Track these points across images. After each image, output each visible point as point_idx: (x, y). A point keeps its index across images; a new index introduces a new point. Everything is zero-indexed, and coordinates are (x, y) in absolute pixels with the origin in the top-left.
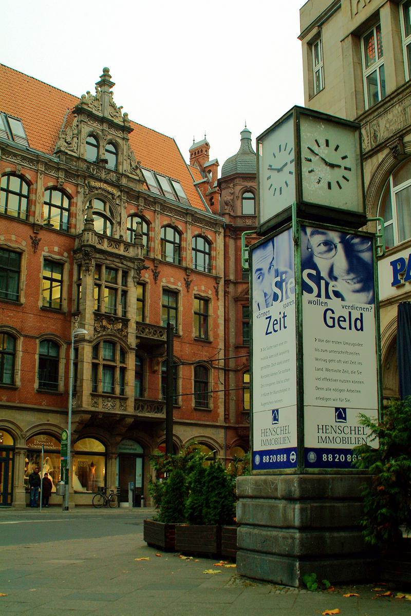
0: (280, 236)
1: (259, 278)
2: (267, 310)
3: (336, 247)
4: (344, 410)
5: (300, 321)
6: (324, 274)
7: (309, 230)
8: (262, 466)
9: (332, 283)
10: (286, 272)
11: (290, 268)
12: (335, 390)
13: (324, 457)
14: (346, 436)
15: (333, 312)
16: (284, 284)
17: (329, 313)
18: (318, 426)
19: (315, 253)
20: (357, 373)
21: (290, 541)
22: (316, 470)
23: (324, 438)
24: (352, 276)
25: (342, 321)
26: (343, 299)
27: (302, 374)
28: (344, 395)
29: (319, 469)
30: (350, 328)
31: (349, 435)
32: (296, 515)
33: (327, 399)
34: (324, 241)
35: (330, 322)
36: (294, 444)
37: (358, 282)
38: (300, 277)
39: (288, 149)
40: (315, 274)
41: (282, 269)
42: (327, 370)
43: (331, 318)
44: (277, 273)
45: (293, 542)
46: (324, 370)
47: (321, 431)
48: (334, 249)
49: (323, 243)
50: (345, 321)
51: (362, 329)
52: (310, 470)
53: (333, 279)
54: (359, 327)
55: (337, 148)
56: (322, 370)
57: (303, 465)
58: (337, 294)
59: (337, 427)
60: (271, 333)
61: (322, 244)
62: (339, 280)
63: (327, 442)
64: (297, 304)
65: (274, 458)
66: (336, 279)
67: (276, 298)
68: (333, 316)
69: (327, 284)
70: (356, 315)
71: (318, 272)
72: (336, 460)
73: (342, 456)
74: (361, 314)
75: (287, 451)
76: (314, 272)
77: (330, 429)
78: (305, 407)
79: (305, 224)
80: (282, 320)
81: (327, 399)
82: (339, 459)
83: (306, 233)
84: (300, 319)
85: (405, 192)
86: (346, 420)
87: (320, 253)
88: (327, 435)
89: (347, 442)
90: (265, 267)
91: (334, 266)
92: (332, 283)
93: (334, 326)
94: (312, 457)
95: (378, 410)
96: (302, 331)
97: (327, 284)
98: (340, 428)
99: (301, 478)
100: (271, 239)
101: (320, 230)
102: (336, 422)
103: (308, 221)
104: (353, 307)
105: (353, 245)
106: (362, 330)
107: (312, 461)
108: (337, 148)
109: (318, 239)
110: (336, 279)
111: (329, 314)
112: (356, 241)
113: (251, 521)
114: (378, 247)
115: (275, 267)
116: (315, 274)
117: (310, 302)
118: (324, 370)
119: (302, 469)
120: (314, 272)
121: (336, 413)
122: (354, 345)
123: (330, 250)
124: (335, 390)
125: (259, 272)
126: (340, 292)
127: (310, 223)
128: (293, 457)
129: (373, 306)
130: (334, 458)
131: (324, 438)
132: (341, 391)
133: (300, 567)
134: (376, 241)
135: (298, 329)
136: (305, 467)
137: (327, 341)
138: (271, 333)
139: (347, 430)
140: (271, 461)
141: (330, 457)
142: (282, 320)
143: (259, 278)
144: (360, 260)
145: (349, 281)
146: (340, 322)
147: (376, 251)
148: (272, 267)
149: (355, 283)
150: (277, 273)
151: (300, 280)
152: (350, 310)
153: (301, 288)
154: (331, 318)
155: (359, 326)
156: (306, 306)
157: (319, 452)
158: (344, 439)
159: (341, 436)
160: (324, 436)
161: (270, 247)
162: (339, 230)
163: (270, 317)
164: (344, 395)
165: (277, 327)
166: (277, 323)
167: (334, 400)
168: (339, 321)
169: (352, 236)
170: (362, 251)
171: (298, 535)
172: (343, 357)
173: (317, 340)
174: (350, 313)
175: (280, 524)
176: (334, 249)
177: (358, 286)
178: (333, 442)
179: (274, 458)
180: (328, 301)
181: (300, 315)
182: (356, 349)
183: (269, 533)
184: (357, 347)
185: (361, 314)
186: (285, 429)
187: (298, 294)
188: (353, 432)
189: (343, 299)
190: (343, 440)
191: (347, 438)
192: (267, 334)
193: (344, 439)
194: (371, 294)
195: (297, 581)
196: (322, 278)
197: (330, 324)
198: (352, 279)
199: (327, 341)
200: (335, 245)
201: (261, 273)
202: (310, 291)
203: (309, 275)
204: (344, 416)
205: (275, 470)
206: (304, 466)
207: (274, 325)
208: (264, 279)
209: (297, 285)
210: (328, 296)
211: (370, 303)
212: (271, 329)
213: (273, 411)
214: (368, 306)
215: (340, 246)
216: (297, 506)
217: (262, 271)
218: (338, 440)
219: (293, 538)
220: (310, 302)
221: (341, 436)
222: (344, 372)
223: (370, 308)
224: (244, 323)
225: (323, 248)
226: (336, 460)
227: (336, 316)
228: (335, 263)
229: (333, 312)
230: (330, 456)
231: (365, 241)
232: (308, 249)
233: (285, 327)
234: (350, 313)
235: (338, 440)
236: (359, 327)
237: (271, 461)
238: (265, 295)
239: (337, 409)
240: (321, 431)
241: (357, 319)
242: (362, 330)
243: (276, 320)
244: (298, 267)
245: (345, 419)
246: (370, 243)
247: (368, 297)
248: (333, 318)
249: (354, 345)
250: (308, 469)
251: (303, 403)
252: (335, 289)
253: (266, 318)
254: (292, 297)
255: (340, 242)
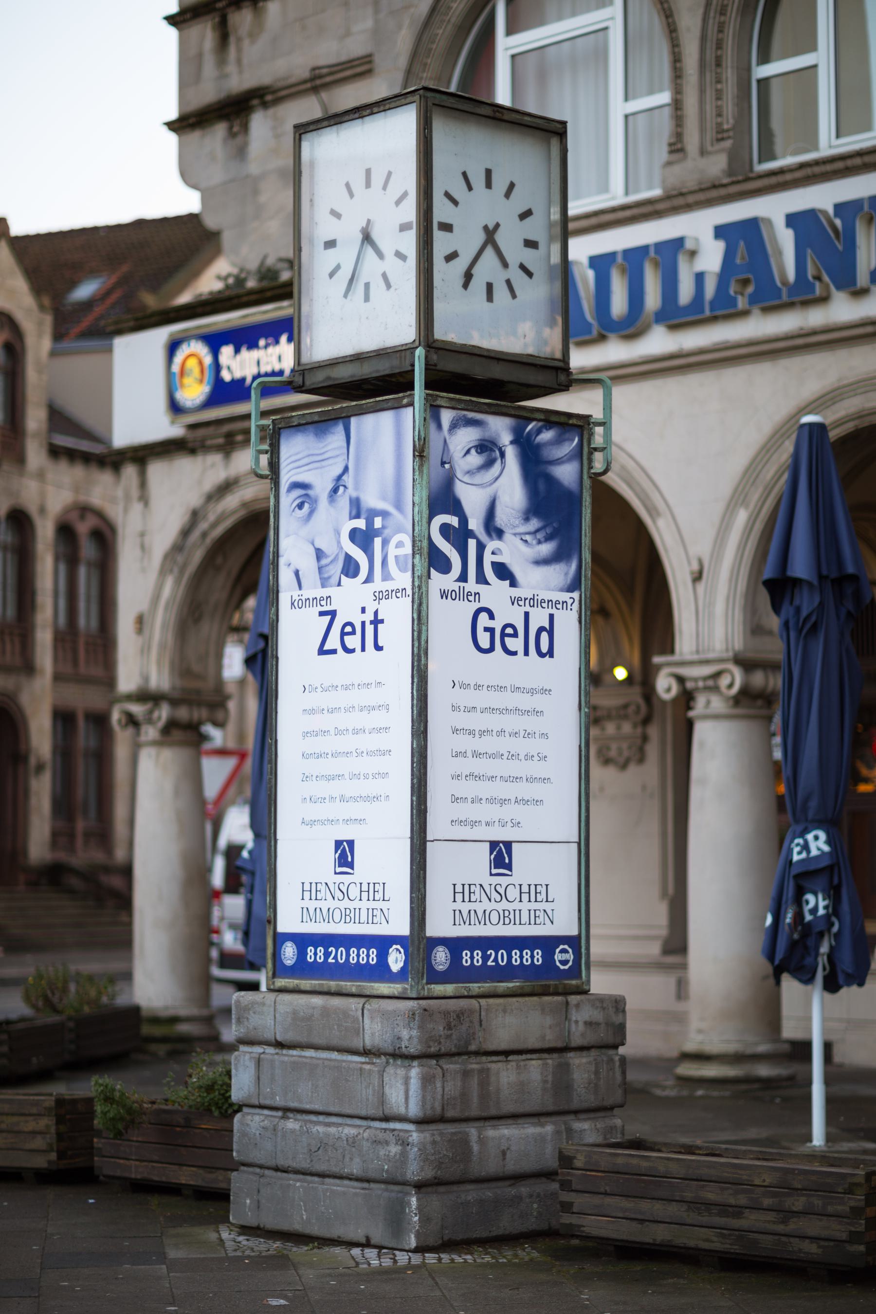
0: (369, 420)
1: (300, 506)
2: (325, 592)
3: (503, 455)
4: (508, 845)
5: (423, 643)
6: (475, 524)
7: (447, 416)
8: (302, 968)
9: (491, 545)
10: (384, 514)
11: (399, 506)
12: (491, 801)
13: (465, 958)
14: (510, 907)
15: (492, 616)
16: (378, 541)
17: (483, 617)
18: (454, 885)
19: (459, 474)
20: (536, 758)
21: (394, 1149)
22: (449, 989)
23: (465, 914)
24: (535, 523)
25: (510, 635)
26: (513, 584)
27: (589, 918)
28: (509, 812)
29: (454, 985)
30: (526, 653)
31: (516, 905)
32: (411, 1093)
33: (474, 823)
34: (476, 443)
35: (484, 640)
36: (401, 926)
37: (548, 538)
38: (426, 536)
39: (394, 190)
40: (457, 526)
41: (372, 500)
42: (476, 754)
43: (486, 629)
44: (356, 509)
45: (404, 1154)
46: (469, 754)
47: (459, 897)
48: (499, 461)
49: (476, 447)
50: (515, 635)
51: (551, 653)
52: (439, 989)
53: (494, 535)
54: (544, 648)
55: (526, 215)
56: (464, 754)
57: (422, 980)
58: (503, 572)
59: (493, 887)
60: (334, 652)
61: (473, 451)
62: (507, 536)
63: (472, 923)
64: (417, 602)
65: (339, 955)
66: (499, 533)
67: (350, 568)
68: (490, 624)
69: (481, 547)
70: (539, 618)
71: (464, 521)
72: (489, 963)
73: (502, 954)
74: (551, 617)
75: (383, 943)
76: (454, 521)
77: (477, 893)
78: (428, 843)
79: (439, 402)
80: (370, 629)
81: (474, 823)
82: (496, 960)
83: (439, 426)
84: (423, 638)
85: (532, 58)
86: (511, 870)
87: (468, 472)
88: (472, 906)
89: (512, 922)
90: (322, 484)
91: (498, 503)
92: (491, 545)
93: (491, 649)
94: (441, 957)
95: (579, 844)
96: (426, 666)
97: (481, 547)
98: (498, 888)
99: (425, 1010)
100: (344, 418)
101: (471, 415)
102: (491, 875)
103: (445, 394)
104: (533, 601)
105: (539, 446)
106: (552, 656)
107: (441, 967)
108: (526, 215)
109: (466, 437)
110: (499, 533)
111: (483, 620)
112: (547, 436)
113: (278, 1101)
114: (595, 449)
115: (352, 492)
116: (457, 526)
117: (444, 594)
118: (469, 754)
119: (420, 987)
120: (454, 521)
121: (491, 853)
122: (532, 691)
123: (489, 464)
124: (491, 801)
125: (299, 492)
126: (509, 566)
127: (451, 399)
128: (396, 960)
129: (576, 595)
130: (485, 958)
131: (465, 914)
132: (503, 802)
133: (420, 1208)
134: (591, 434)
135: (419, 660)
136: (427, 983)
137: (478, 687)
138: (334, 652)
139: (513, 893)
140: (330, 960)
141: (478, 955)
142: (370, 629)
143: (300, 506)
144: (552, 481)
145: (528, 538)
146: (507, 639)
147: (590, 461)
148: (341, 489)
149: (539, 542)
150: (356, 509)
151: (425, 544)
152: (527, 608)
153: (426, 564)
154: (486, 629)
155: (544, 647)
156: (436, 606)
157: (455, 945)
158: (507, 913)
159: (502, 906)
160: (465, 907)
161: (335, 438)
162: (513, 412)
163: (333, 614)
164: (509, 812)
165: (353, 641)
166: (323, 600)
167: (487, 824)
168: (503, 635)
169: (540, 424)
170: (558, 462)
171: (415, 1136)
172: (511, 722)
173: (457, 686)
174: (527, 615)
175: (371, 1112)
176: (499, 461)
177: (546, 549)
178: (483, 922)
179: (339, 955)
180: (481, 588)
181: (424, 628)
182: (537, 702)
183: (332, 1130)
184: (539, 695)
185: (551, 617)
186: (373, 890)
187: (420, 578)
188: (525, 897)
189: (513, 584)
190: (504, 917)
191: (512, 913)
192: (322, 652)
193: (507, 913)
194: (574, 566)
195: (413, 1236)
196: (471, 534)
197: (485, 642)
198: (537, 531)
199: (478, 687)
200: (500, 449)
201: (307, 495)
202: (444, 566)
203: (445, 530)
204: (507, 861)
205: (340, 983)
206: (425, 981)
207: (343, 634)
208: (316, 516)
209: (418, 556)
210: (481, 579)
211: (570, 589)
212: (333, 642)
213: (338, 844)
214: (565, 596)
215: (511, 453)
216: (415, 1072)
217: (310, 492)
218: (494, 917)
219: (404, 1143)
220: (444, 594)
221: (502, 906)
222: (512, 756)
223: (570, 601)
224: (473, 802)
225: (475, 459)
226: (489, 963)
227: (497, 625)
228: (500, 493)
229: (492, 616)
230: (478, 955)
231: (567, 436)
232: (443, 463)
233: (378, 648)
234: (527, 615)
235: (494, 917)
236: (544, 648)
237: (330, 960)
238: (319, 554)
239: (494, 845)
240: (459, 897)
241: (541, 629)
242: (552, 656)
243: (349, 624)
244: (420, 512)
245: (509, 867)
246: (576, 440)
247: (566, 574)
248: (491, 630)
249: (532, 691)
250: (433, 986)
251: (425, 837)
252: (497, 559)
253: (322, 614)
254: (403, 580)
255: (512, 443)
